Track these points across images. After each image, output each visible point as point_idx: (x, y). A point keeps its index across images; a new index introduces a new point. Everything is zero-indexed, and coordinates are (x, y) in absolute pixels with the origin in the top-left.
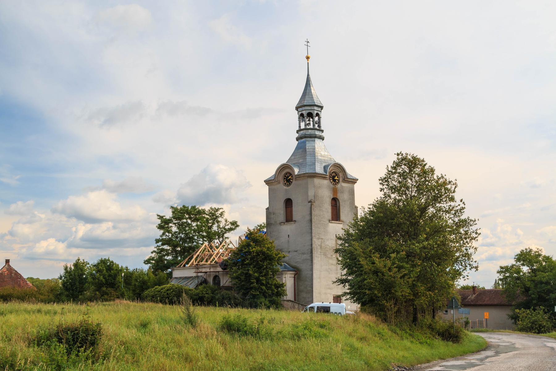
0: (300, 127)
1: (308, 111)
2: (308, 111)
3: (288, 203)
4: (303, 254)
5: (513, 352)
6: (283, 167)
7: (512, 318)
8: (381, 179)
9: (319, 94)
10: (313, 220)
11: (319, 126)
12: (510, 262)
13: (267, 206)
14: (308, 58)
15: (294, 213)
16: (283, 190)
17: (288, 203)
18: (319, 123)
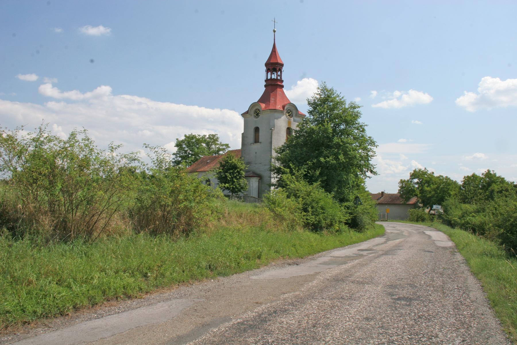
0: (267, 78)
1: (274, 65)
2: (274, 65)
3: (257, 130)
4: (265, 165)
5: (398, 240)
6: (253, 105)
7: (187, 235)
8: (401, 180)
9: (283, 57)
10: (273, 142)
11: (281, 78)
12: (407, 177)
13: (243, 132)
14: (274, 31)
15: (260, 137)
16: (254, 122)
17: (257, 130)
18: (281, 76)
